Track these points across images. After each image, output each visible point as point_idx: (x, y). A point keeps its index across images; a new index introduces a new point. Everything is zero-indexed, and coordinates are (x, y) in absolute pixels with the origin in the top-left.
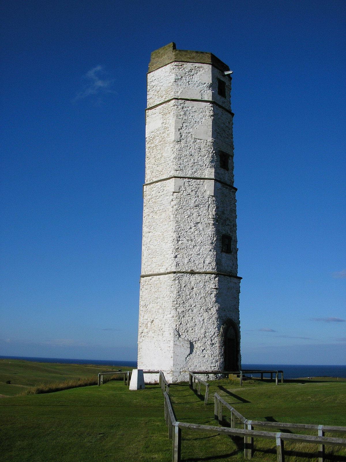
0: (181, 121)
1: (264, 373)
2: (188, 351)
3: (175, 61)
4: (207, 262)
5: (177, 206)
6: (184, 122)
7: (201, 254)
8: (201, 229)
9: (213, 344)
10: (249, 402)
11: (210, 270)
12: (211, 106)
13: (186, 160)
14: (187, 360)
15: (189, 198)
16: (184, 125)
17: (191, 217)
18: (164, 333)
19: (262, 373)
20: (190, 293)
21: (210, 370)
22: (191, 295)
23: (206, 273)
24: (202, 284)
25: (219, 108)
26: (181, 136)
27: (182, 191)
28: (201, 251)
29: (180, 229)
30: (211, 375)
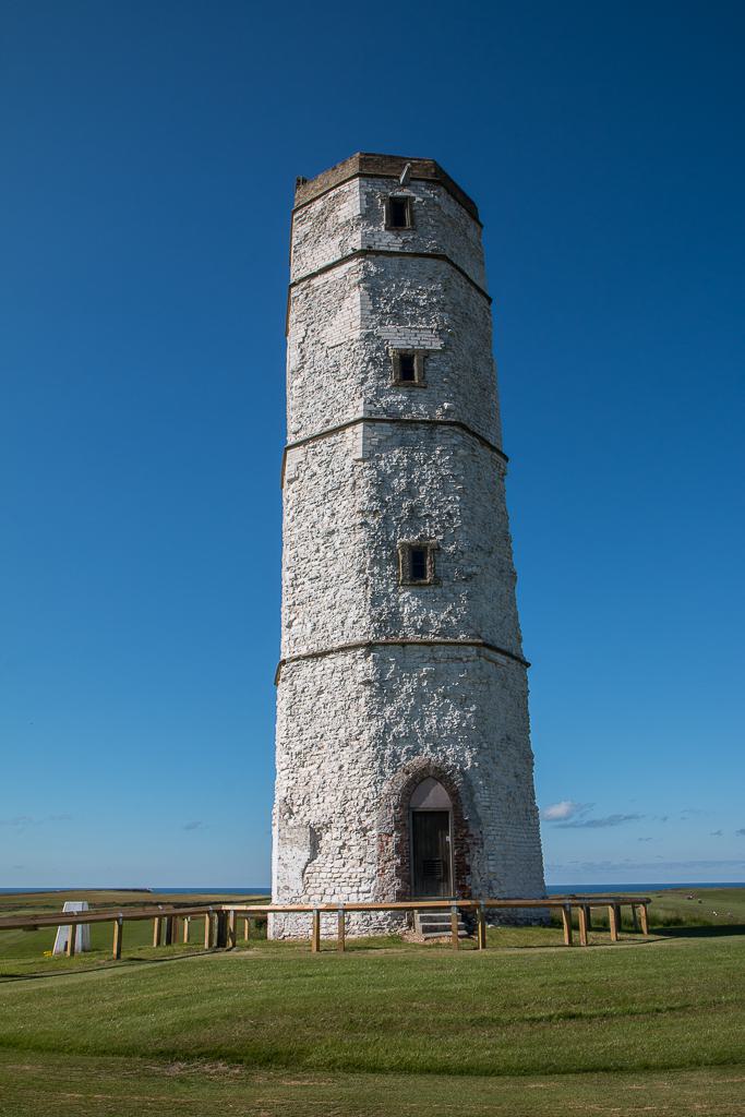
2: (306, 855)
7: (337, 605)
14: (306, 876)
26: (303, 357)
28: (338, 598)
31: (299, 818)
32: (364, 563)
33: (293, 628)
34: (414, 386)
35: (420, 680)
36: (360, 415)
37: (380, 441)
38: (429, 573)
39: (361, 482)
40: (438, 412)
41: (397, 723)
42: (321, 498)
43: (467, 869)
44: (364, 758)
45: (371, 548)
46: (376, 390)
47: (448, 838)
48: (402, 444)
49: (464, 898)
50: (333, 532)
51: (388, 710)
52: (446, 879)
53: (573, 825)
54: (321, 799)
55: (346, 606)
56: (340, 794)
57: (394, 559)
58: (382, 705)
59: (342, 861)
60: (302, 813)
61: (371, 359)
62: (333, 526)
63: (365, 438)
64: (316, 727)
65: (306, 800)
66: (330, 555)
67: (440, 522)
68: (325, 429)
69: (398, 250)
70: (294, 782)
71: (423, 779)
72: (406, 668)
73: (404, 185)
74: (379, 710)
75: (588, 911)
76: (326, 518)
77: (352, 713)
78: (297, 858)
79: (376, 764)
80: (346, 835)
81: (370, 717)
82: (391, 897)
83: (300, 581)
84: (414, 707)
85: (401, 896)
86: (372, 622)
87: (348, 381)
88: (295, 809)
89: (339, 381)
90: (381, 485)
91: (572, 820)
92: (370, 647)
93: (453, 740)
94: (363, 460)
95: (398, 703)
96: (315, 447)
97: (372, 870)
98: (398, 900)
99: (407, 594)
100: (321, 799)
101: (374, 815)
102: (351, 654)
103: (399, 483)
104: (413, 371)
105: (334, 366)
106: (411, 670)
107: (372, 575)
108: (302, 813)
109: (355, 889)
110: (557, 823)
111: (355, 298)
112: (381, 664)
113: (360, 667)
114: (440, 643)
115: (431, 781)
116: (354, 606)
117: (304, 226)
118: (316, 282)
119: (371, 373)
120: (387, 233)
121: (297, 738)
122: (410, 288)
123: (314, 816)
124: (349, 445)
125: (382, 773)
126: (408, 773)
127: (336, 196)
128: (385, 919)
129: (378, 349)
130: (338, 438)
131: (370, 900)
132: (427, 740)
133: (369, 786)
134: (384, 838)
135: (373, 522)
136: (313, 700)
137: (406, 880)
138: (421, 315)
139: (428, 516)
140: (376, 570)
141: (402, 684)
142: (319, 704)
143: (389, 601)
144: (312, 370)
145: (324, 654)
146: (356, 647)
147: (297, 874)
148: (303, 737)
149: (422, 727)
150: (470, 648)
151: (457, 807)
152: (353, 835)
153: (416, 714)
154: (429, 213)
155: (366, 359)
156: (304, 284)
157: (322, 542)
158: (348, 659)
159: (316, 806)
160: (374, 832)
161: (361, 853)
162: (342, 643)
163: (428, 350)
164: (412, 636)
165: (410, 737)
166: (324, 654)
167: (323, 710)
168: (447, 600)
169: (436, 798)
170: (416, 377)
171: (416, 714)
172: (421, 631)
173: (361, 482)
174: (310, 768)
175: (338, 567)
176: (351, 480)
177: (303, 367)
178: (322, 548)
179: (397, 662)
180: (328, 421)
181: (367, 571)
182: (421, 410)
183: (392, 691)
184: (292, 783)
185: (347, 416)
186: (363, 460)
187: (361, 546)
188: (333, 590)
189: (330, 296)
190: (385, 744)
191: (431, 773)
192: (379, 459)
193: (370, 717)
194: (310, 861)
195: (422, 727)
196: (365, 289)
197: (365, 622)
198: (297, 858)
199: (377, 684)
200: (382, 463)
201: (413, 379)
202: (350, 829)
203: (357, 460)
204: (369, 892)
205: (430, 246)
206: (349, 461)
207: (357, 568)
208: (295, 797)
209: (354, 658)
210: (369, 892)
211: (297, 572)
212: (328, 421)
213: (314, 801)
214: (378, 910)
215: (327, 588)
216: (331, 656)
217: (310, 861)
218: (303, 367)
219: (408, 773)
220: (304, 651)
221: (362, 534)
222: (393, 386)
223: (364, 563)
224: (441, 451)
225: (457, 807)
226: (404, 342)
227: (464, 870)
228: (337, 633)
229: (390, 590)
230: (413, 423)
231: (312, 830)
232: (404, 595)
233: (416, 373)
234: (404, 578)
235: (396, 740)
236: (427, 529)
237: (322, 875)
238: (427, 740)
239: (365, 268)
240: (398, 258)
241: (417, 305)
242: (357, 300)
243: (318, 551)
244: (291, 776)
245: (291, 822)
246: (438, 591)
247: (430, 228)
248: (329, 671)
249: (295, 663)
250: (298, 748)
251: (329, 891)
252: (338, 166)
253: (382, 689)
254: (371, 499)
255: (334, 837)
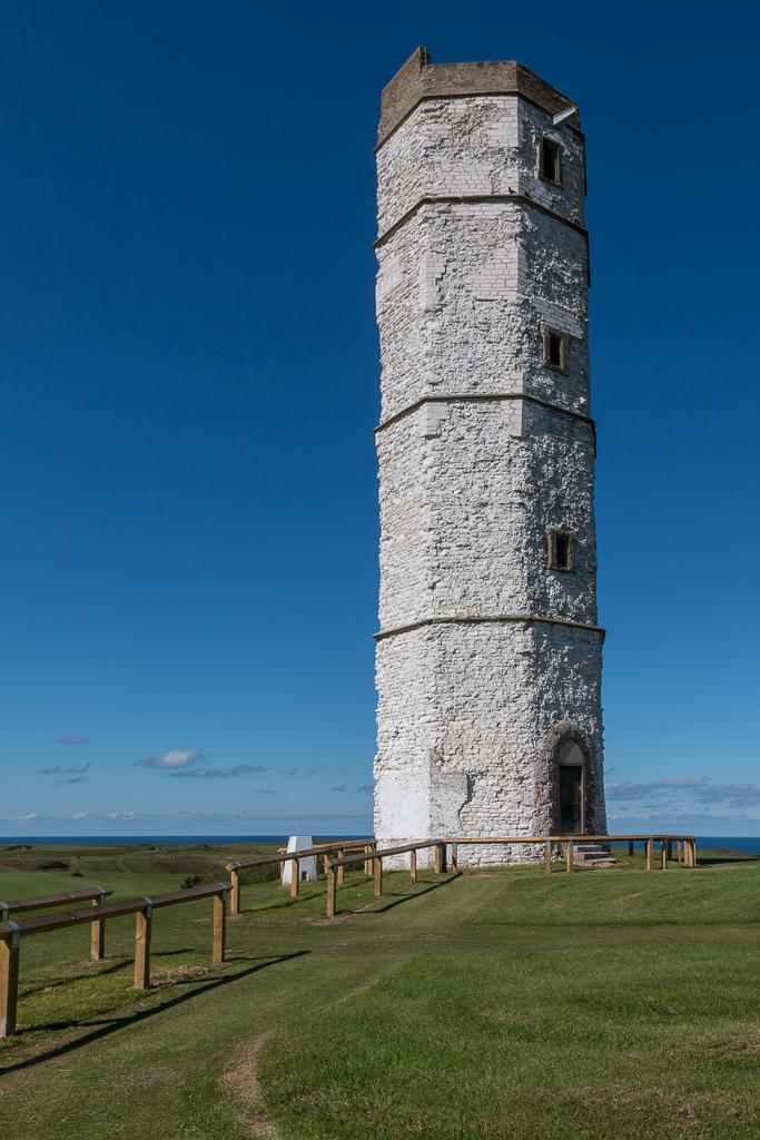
0: (442, 259)
1: (302, 857)
2: (464, 797)
3: (425, 99)
4: (505, 595)
5: (435, 468)
6: (448, 261)
7: (492, 575)
8: (491, 518)
9: (522, 779)
10: (309, 952)
11: (515, 611)
12: (517, 211)
13: (456, 355)
14: (461, 815)
15: (463, 446)
16: (449, 270)
17: (468, 493)
18: (415, 758)
19: (414, 850)
20: (467, 667)
21: (513, 835)
22: (468, 670)
23: (503, 620)
24: (493, 644)
25: (540, 215)
26: (442, 298)
27: (446, 433)
28: (491, 570)
29: (441, 522)
30: (516, 848)
31: (452, 766)
32: (520, 542)
33: (435, 591)
34: (559, 371)
35: (563, 656)
36: (519, 390)
37: (534, 423)
38: (569, 561)
39: (518, 461)
40: (576, 405)
41: (547, 691)
42: (470, 465)
43: (593, 811)
44: (523, 718)
45: (528, 529)
46: (530, 366)
47: (581, 788)
48: (551, 430)
49: (590, 834)
50: (485, 505)
51: (541, 679)
52: (578, 820)
53: (190, 775)
54: (476, 751)
55: (502, 580)
56: (497, 748)
57: (544, 544)
58: (537, 674)
59: (500, 803)
60: (455, 762)
61: (527, 331)
62: (485, 497)
63: (524, 417)
64: (470, 685)
65: (460, 750)
66: (481, 526)
67: (576, 515)
68: (471, 393)
69: (548, 207)
70: (444, 734)
71: (567, 740)
72: (555, 645)
73: (557, 128)
74: (534, 679)
75: (455, 851)
76: (475, 487)
77: (509, 679)
78: (452, 799)
79: (534, 724)
80: (503, 782)
81: (528, 684)
82: (546, 832)
83: (444, 545)
84: (558, 678)
85: (552, 832)
86: (528, 599)
87: (501, 347)
88: (446, 758)
89: (490, 342)
90: (535, 469)
91: (190, 769)
92: (530, 622)
93: (582, 709)
94: (520, 439)
95: (548, 674)
96: (462, 408)
97: (530, 811)
98: (551, 835)
99: (552, 578)
100: (476, 751)
101: (531, 767)
102: (511, 625)
103: (548, 470)
104: (558, 355)
105: (485, 324)
106: (559, 646)
107: (527, 554)
108: (455, 762)
109: (515, 826)
110: (176, 771)
111: (511, 252)
112: (537, 638)
113: (519, 638)
114: (576, 626)
115: (571, 742)
116: (511, 581)
117: (437, 126)
118: (459, 209)
119: (527, 346)
120: (540, 183)
121: (448, 695)
122: (557, 258)
123: (469, 764)
124: (503, 418)
125: (538, 733)
126: (556, 733)
127: (485, 108)
128: (541, 850)
129: (532, 321)
130: (492, 407)
131: (529, 836)
132: (567, 707)
133: (527, 742)
134: (540, 786)
135: (530, 504)
136: (467, 662)
137: (556, 820)
138: (565, 294)
139: (568, 507)
140: (530, 551)
141: (551, 658)
142: (474, 666)
143: (539, 581)
144: (454, 318)
145: (479, 621)
146: (517, 620)
147: (453, 813)
148: (455, 694)
149: (563, 697)
150: (596, 634)
151: (587, 764)
152: (511, 783)
153: (559, 686)
154: (574, 173)
155: (523, 328)
156: (444, 207)
157: (474, 511)
158: (506, 630)
159: (471, 756)
160: (530, 780)
161: (519, 798)
162: (497, 614)
163: (572, 336)
164: (556, 617)
165: (556, 705)
166: (479, 621)
167: (477, 672)
168: (582, 589)
169: (574, 756)
170: (562, 363)
171: (559, 686)
172: (561, 613)
173: (518, 461)
174: (463, 723)
175: (491, 540)
176: (506, 456)
177: (441, 310)
178: (472, 518)
179: (549, 639)
180: (476, 384)
181: (523, 551)
182: (561, 400)
183: (543, 663)
184: (442, 735)
185: (499, 385)
186: (520, 439)
187: (520, 525)
188: (485, 562)
189: (477, 236)
190: (539, 708)
191: (572, 735)
192: (533, 441)
193: (528, 684)
194: (466, 802)
195: (563, 697)
196: (522, 245)
197: (522, 597)
198: (452, 799)
199: (534, 656)
200: (535, 446)
201: (558, 364)
202: (507, 777)
203: (514, 438)
204: (527, 828)
205: (573, 214)
206: (504, 437)
207: (515, 545)
208: (447, 748)
209: (512, 629)
210: (527, 828)
211: (442, 535)
212: (476, 384)
213: (467, 751)
214: (535, 842)
215: (478, 558)
216: (487, 624)
217: (466, 802)
218: (441, 310)
219: (556, 733)
220: (452, 614)
221: (519, 514)
222: (544, 367)
223: (520, 542)
224: (579, 446)
225: (587, 764)
226: (553, 321)
227: (590, 813)
228: (491, 603)
229: (540, 571)
230: (556, 410)
231: (468, 777)
232: (549, 578)
233: (561, 359)
234: (553, 564)
235: (547, 707)
236: (569, 520)
237: (478, 814)
238: (567, 707)
239: (522, 220)
240: (551, 219)
241: (562, 281)
242: (515, 255)
243: (467, 519)
244: (441, 728)
245: (444, 769)
246: (573, 579)
247: (572, 191)
248: (484, 638)
249: (446, 625)
250: (449, 704)
251: (486, 828)
252: (486, 63)
253: (538, 661)
254: (528, 481)
255: (490, 783)
